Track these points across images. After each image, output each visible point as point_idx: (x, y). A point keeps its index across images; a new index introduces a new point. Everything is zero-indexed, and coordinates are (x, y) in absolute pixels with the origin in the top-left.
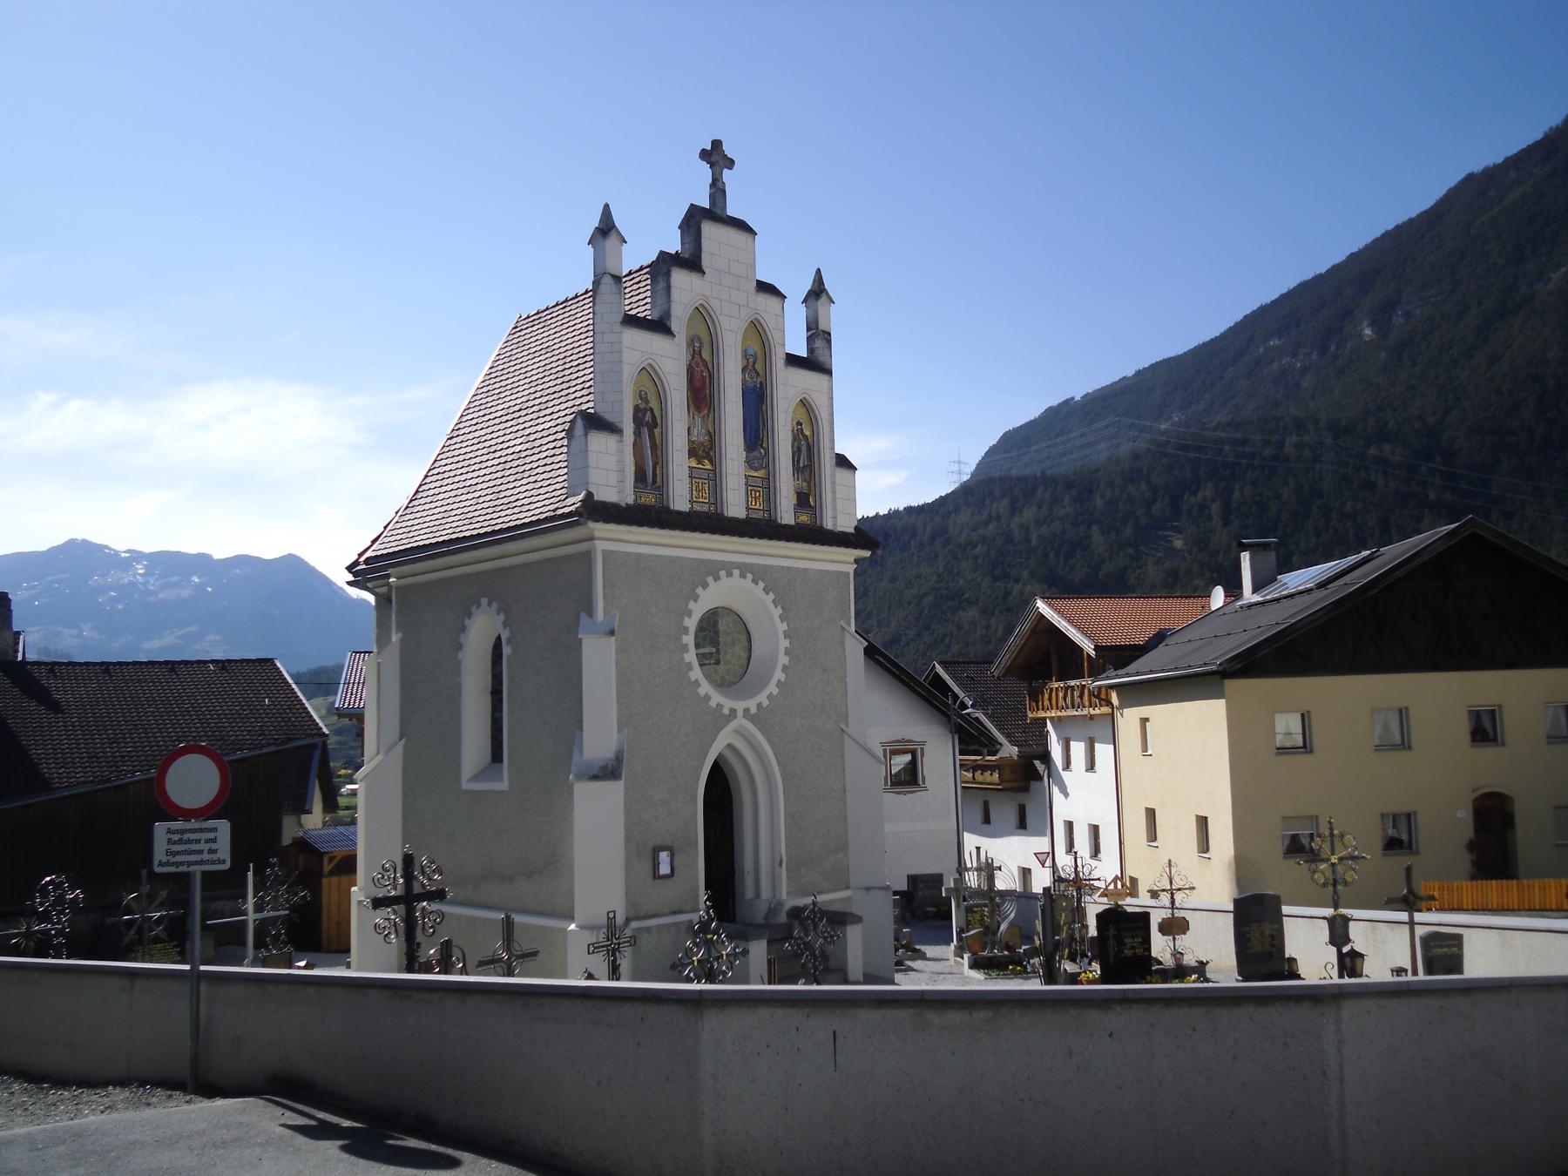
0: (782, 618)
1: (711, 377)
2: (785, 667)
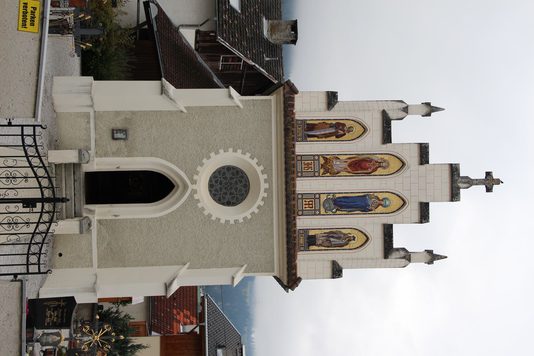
0: (245, 218)
1: (368, 174)
2: (253, 213)
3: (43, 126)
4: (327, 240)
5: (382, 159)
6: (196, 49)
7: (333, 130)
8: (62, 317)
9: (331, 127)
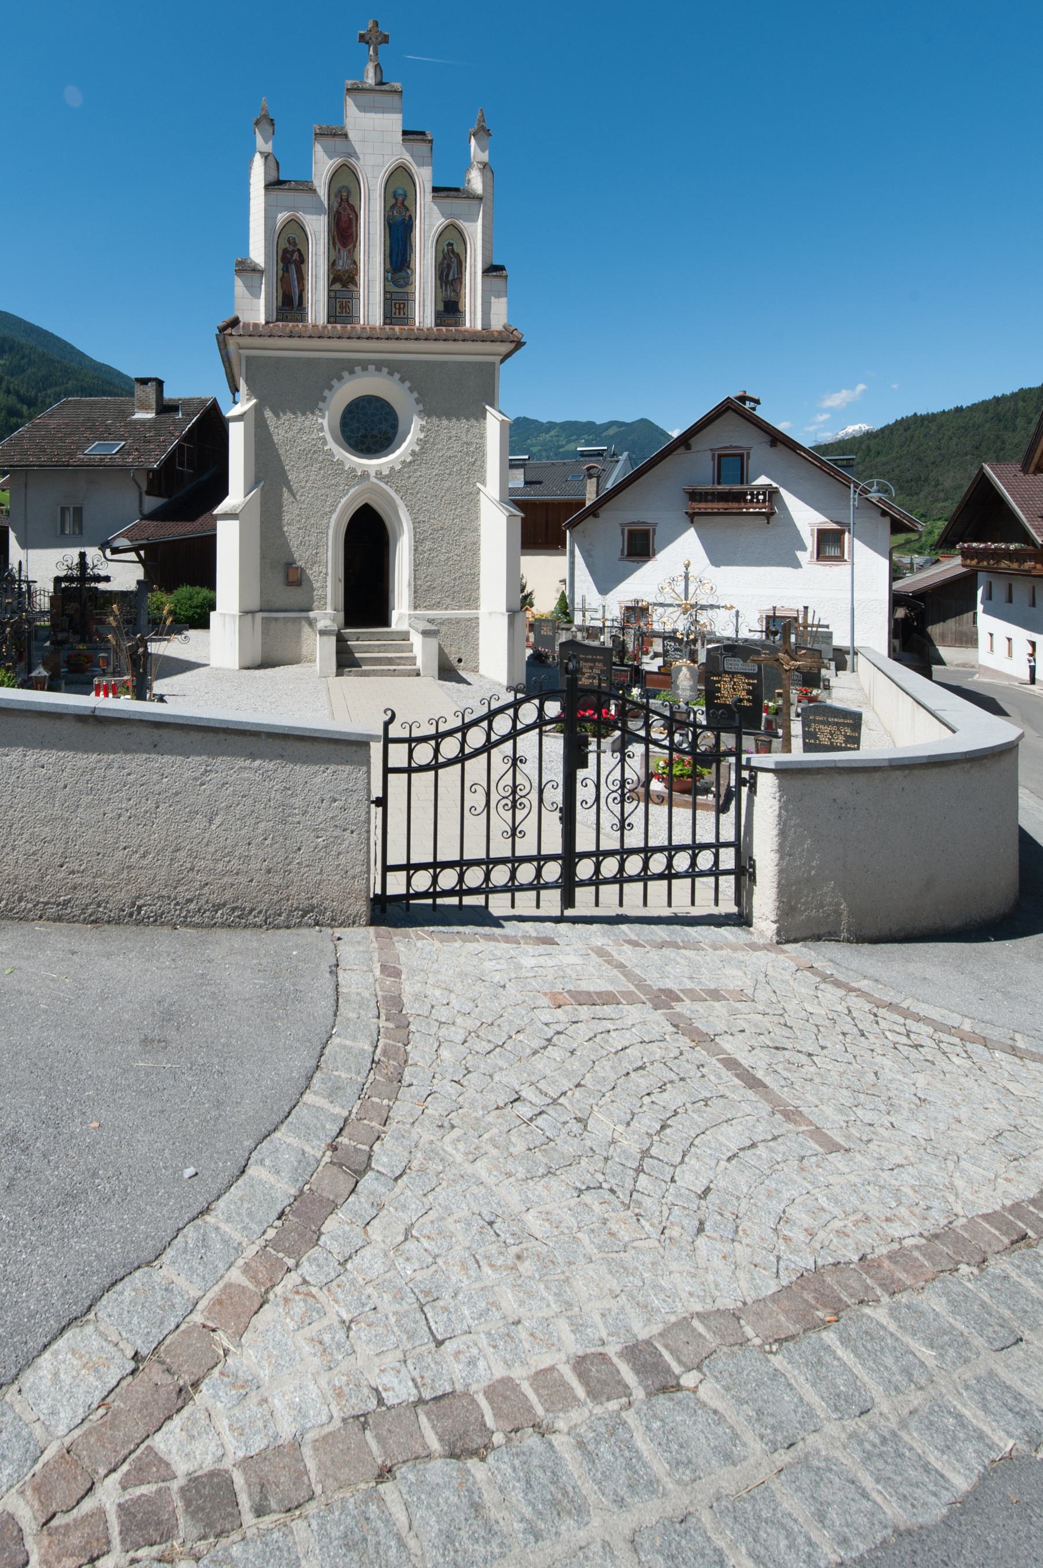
3: (387, 718)
4: (452, 284)
5: (336, 197)
6: (169, 497)
7: (293, 268)
8: (593, 661)
9: (287, 271)
